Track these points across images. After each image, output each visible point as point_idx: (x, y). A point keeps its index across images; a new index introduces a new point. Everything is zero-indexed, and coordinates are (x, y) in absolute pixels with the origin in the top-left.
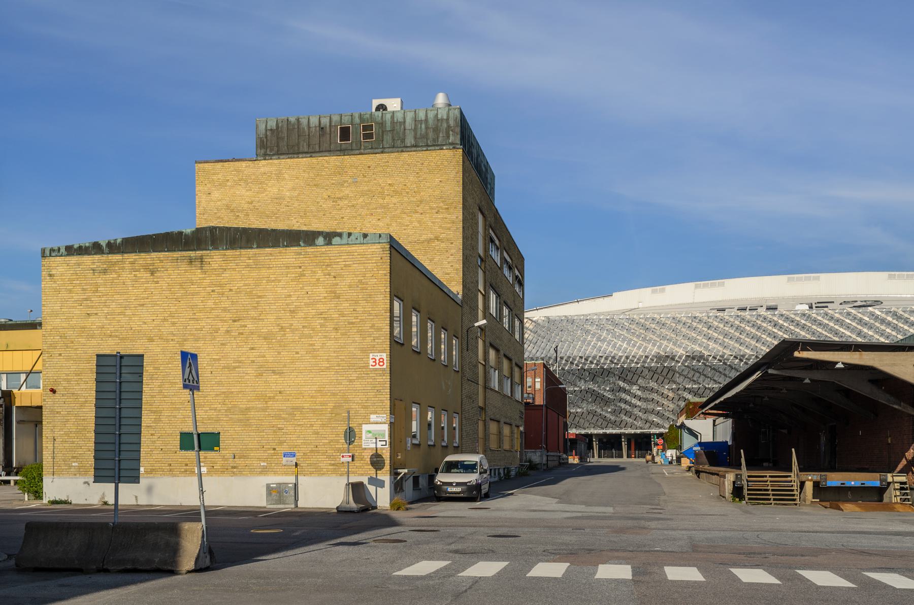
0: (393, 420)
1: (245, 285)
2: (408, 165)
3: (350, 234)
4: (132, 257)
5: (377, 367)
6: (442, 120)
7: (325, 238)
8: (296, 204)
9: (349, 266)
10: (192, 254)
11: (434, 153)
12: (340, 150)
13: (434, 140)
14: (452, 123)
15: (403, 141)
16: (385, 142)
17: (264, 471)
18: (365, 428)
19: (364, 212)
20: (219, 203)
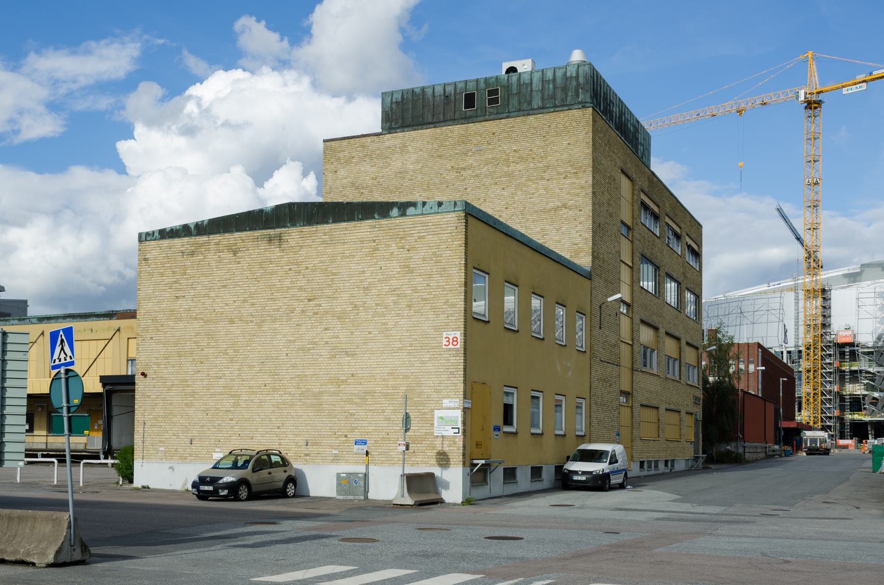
0: (468, 405)
1: (321, 262)
2: (535, 128)
3: (424, 204)
4: (216, 238)
5: (451, 346)
6: (571, 77)
7: (399, 209)
8: (419, 178)
9: (423, 237)
10: (271, 232)
11: (562, 115)
12: (465, 118)
13: (562, 100)
14: (581, 80)
15: (530, 103)
16: (510, 107)
17: (336, 459)
18: (438, 413)
19: (488, 181)
20: (345, 181)
